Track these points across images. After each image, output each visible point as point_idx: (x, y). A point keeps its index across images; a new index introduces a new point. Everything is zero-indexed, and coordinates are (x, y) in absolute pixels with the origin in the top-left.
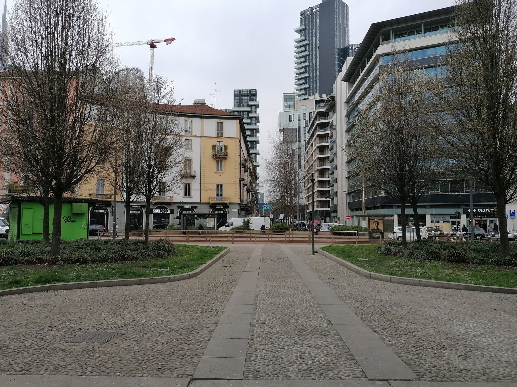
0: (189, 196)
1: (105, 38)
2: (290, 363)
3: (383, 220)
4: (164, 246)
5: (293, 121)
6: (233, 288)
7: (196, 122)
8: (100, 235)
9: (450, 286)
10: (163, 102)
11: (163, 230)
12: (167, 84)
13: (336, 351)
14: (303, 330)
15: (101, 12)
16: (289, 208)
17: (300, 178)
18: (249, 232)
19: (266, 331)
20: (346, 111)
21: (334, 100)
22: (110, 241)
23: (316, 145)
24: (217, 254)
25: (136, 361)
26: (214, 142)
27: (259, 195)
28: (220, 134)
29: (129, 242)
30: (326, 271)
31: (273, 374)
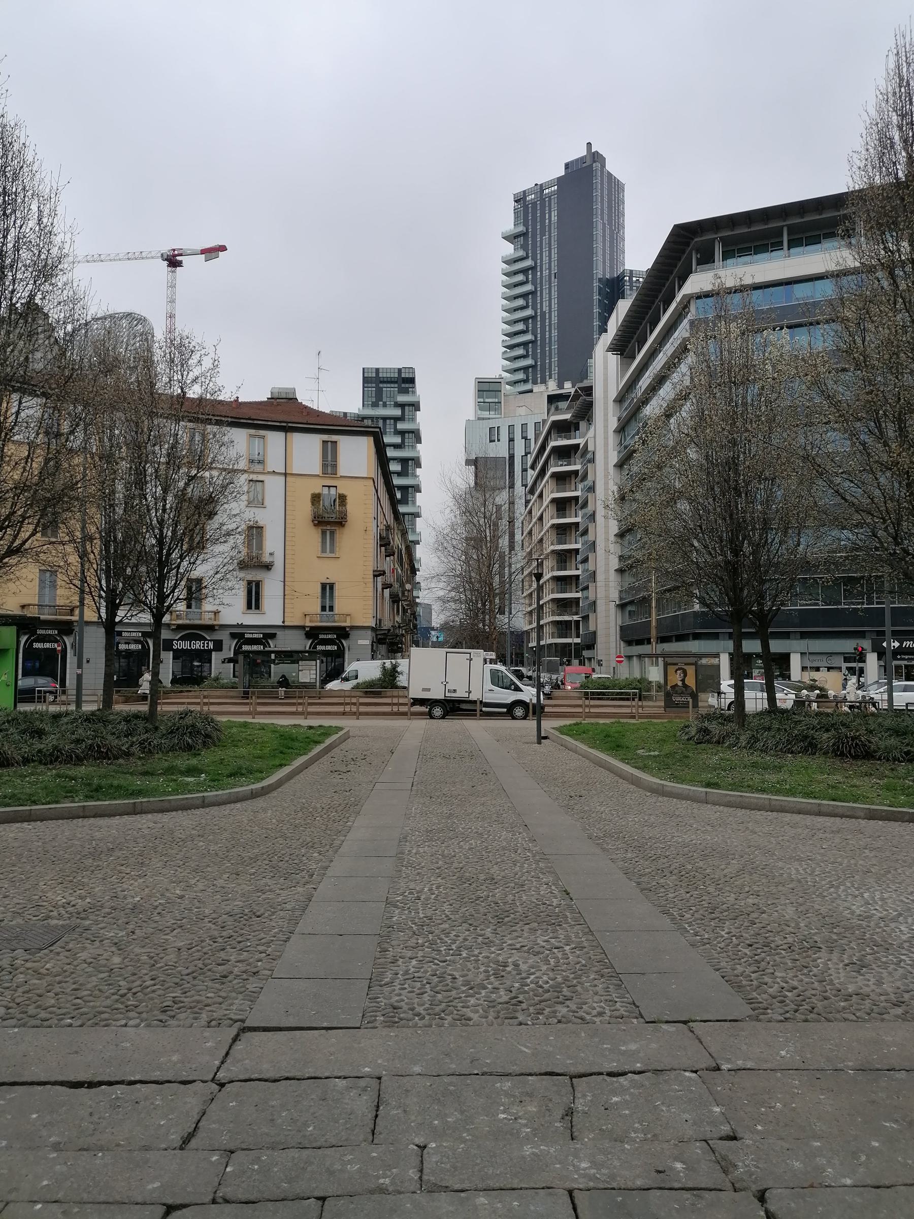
0: (257, 611)
1: (57, 240)
2: (471, 989)
3: (695, 664)
4: (193, 726)
5: (499, 440)
6: (351, 819)
7: (275, 439)
8: (45, 702)
9: (837, 811)
10: (194, 392)
11: (196, 688)
12: (203, 352)
13: (576, 959)
14: (506, 914)
15: (47, 180)
16: (488, 638)
17: (513, 571)
18: (395, 692)
19: (421, 916)
20: (616, 419)
21: (590, 395)
22: (67, 714)
23: (548, 497)
24: (317, 742)
25: (112, 991)
26: (316, 487)
27: (420, 610)
28: (329, 468)
29: (112, 717)
30: (565, 780)
31: (429, 1014)
